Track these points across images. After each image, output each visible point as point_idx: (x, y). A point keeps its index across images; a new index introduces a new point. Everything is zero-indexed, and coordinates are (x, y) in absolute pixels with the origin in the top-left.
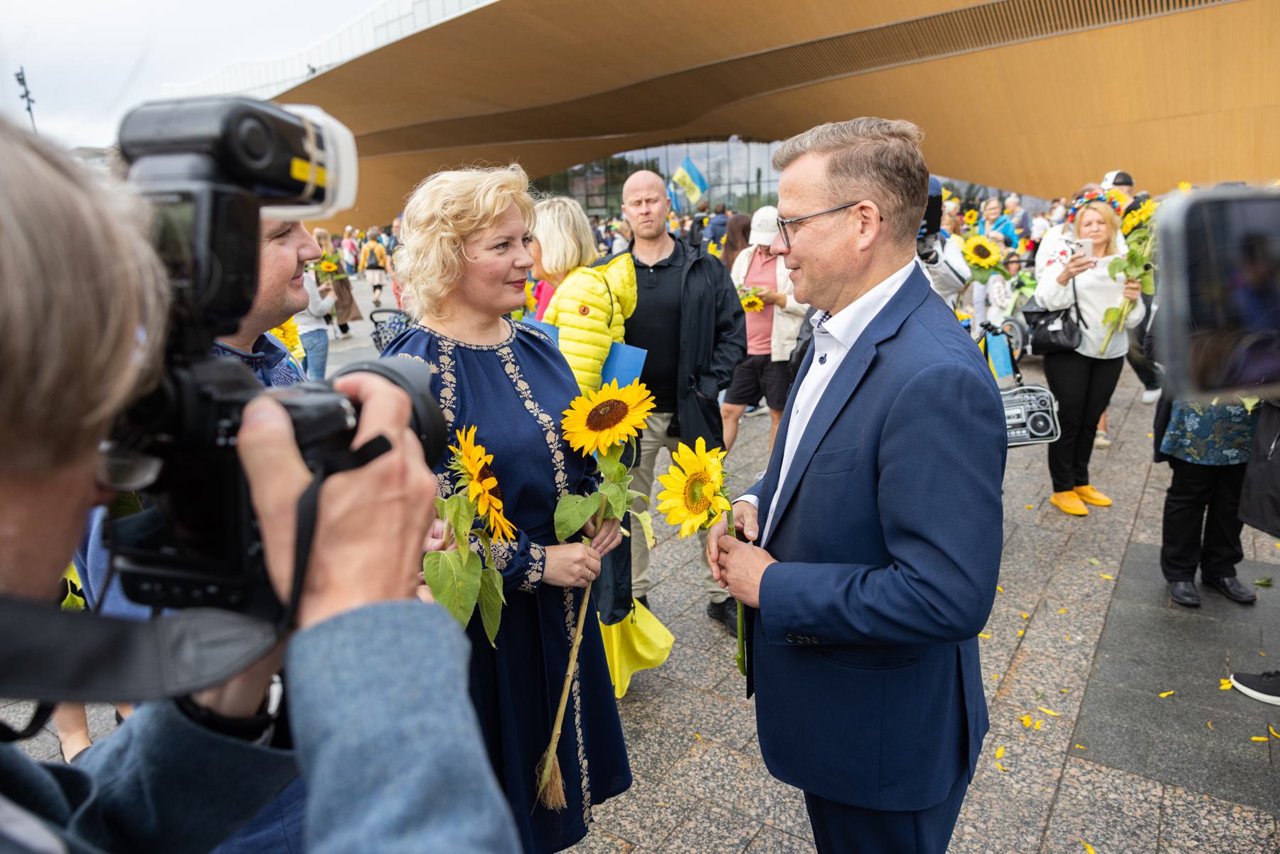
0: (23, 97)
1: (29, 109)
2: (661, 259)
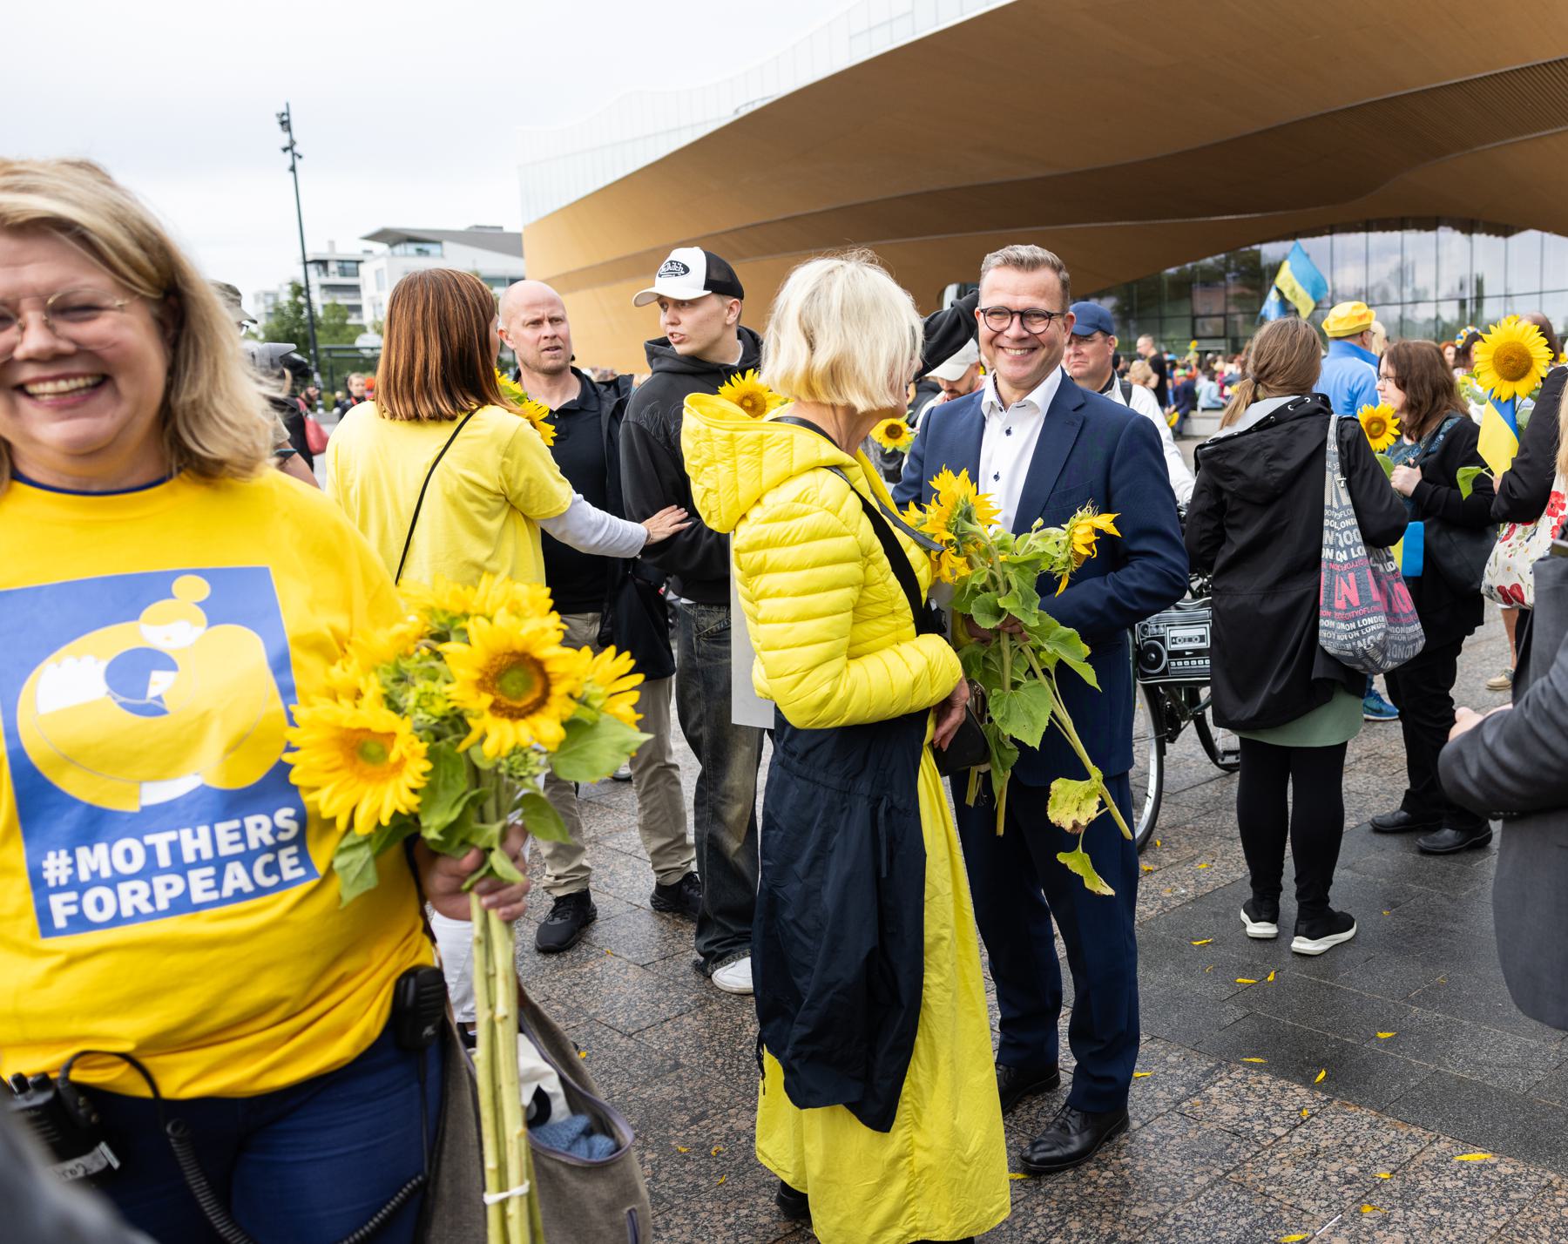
0: (285, 150)
1: (293, 169)
2: (565, 402)
